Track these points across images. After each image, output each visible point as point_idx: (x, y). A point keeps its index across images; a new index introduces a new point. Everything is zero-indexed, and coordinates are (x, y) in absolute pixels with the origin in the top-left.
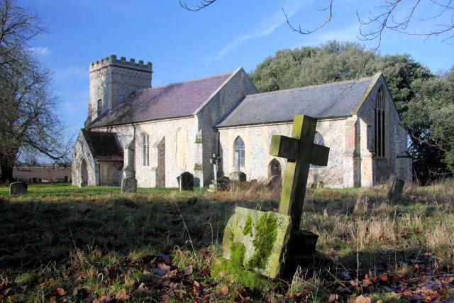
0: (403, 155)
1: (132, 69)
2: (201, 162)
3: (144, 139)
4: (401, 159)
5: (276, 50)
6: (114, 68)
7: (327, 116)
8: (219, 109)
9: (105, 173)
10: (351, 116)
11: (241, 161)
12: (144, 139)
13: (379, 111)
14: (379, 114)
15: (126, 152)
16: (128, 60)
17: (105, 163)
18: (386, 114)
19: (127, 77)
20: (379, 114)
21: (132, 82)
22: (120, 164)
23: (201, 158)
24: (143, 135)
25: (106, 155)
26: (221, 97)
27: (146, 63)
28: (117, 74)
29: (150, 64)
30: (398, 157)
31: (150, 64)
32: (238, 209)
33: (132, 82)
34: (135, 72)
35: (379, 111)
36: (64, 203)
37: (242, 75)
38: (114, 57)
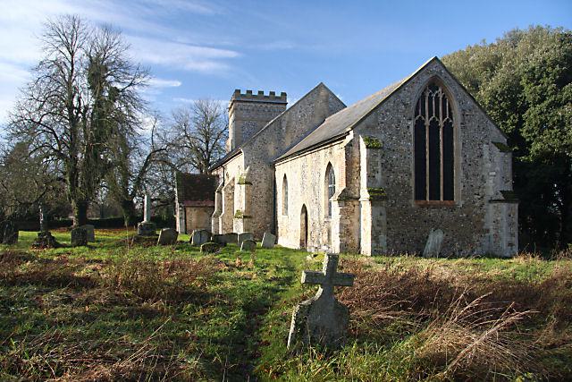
2: (244, 209)
5: (509, 28)
8: (280, 139)
9: (194, 220)
13: (434, 124)
16: (267, 94)
17: (193, 209)
18: (457, 125)
21: (261, 116)
23: (244, 202)
25: (195, 200)
27: (278, 94)
28: (241, 109)
30: (490, 201)
31: (284, 94)
33: (261, 116)
34: (264, 105)
35: (434, 124)
36: (27, 274)
37: (323, 93)
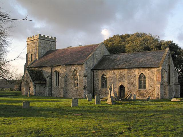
0: (176, 83)
1: (47, 40)
3: (57, 73)
4: (176, 85)
6: (40, 40)
7: (77, 63)
9: (38, 89)
10: (159, 67)
11: (85, 92)
12: (57, 73)
14: (168, 66)
15: (48, 80)
19: (45, 44)
20: (168, 66)
22: (45, 85)
24: (56, 71)
26: (94, 55)
29: (55, 38)
30: (174, 84)
32: (112, 95)
38: (40, 35)
